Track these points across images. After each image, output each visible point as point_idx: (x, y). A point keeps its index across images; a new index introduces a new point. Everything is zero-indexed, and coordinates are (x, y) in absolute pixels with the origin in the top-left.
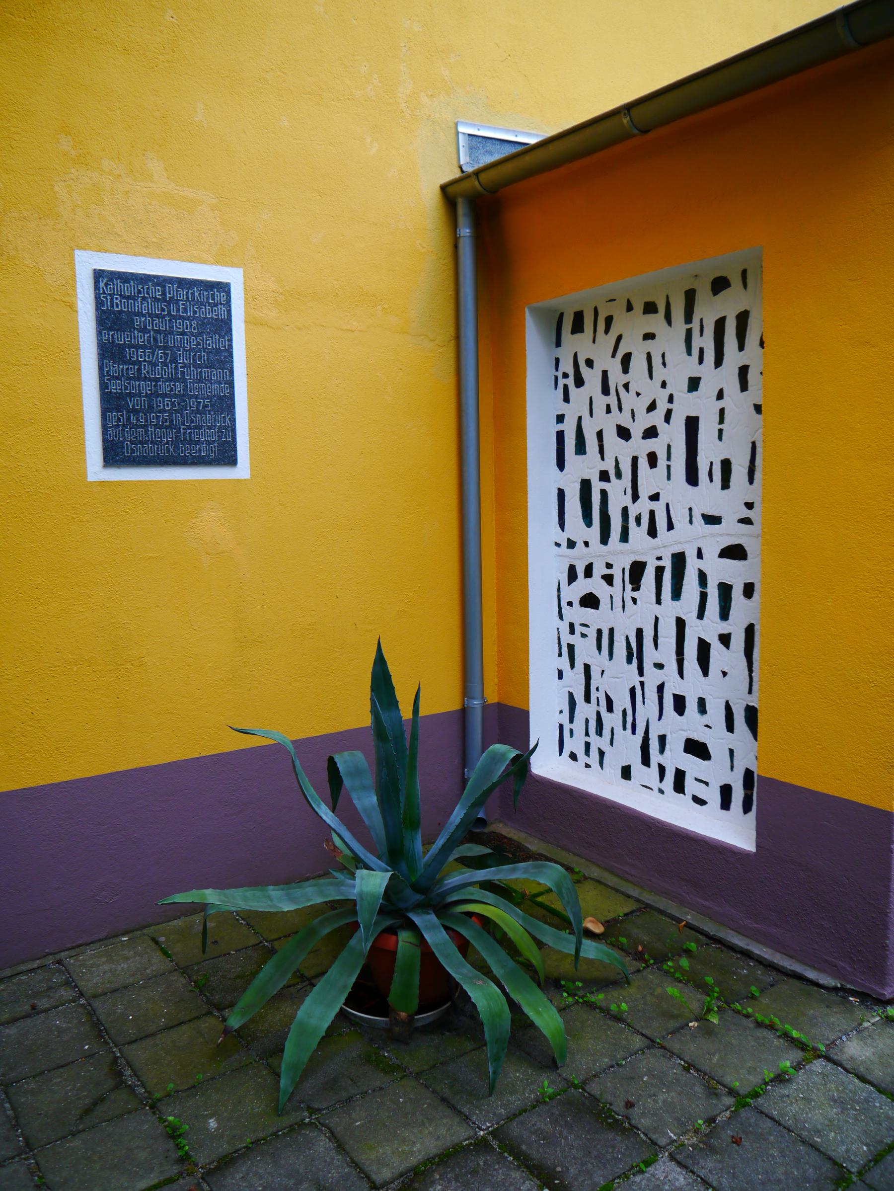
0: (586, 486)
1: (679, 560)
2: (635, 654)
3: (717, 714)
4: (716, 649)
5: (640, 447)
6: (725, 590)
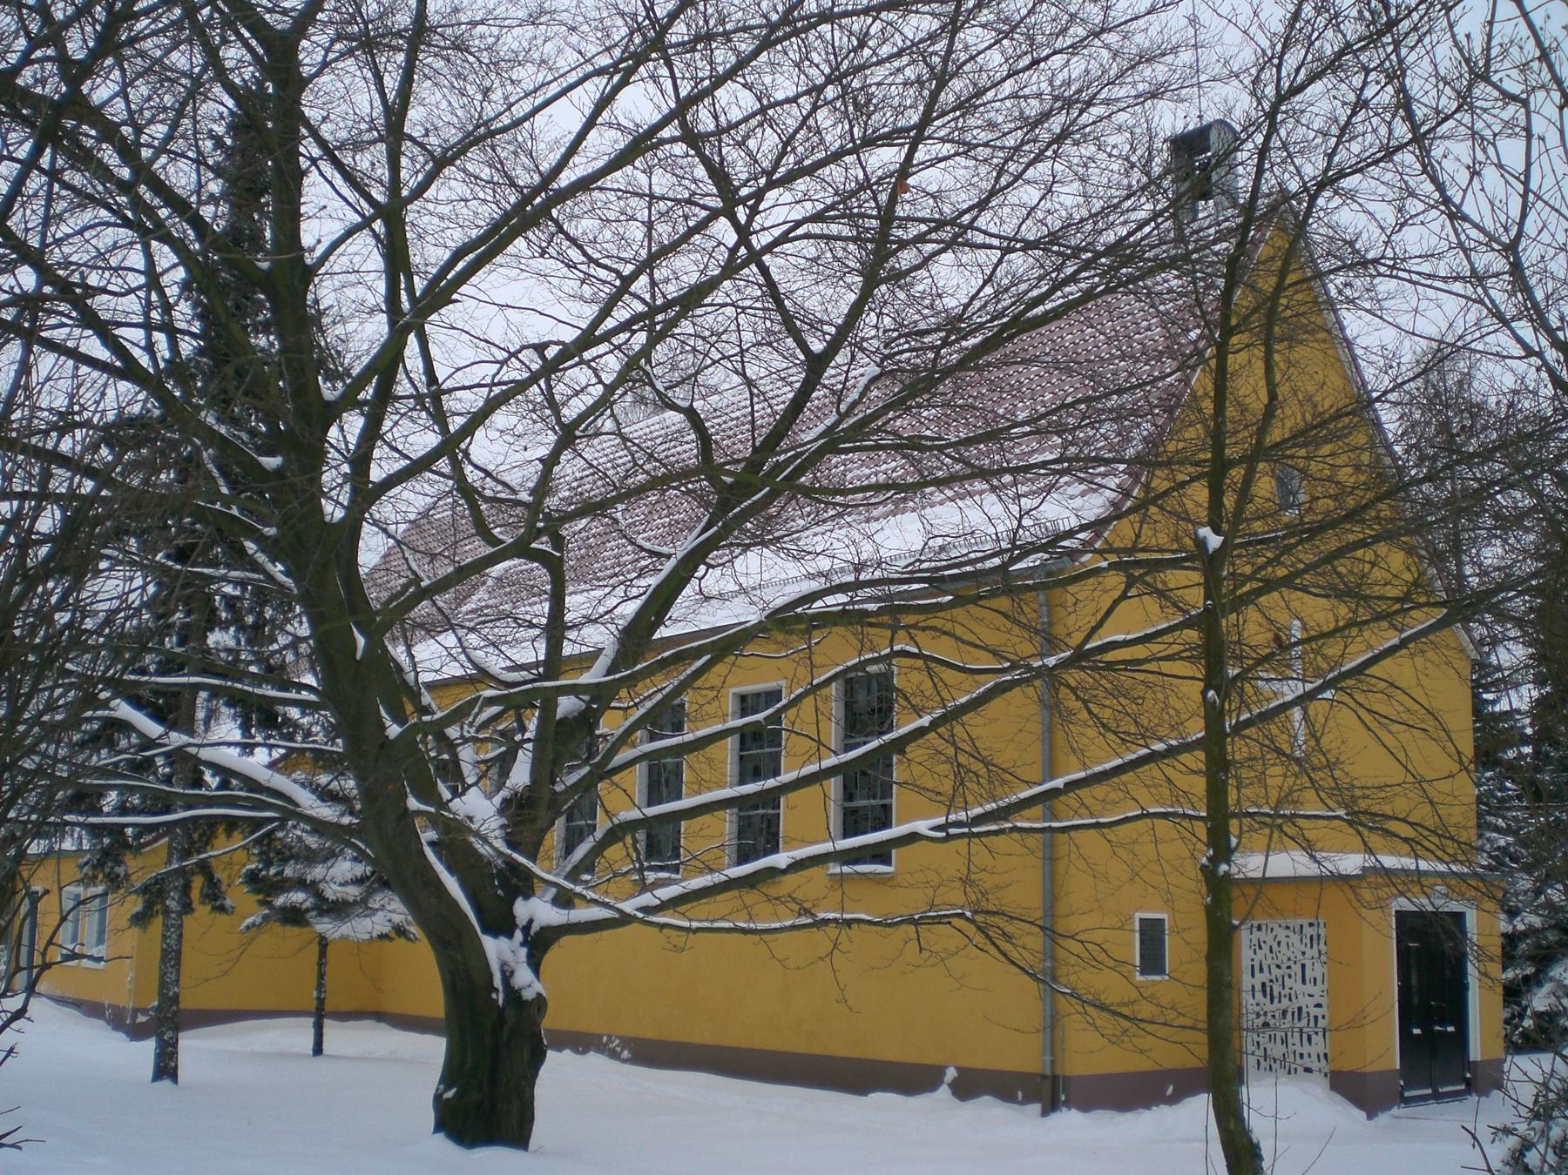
0: (1264, 984)
1: (1300, 1009)
2: (1285, 1041)
3: (1314, 1057)
4: (1314, 1037)
5: (1284, 970)
6: (1316, 1018)
